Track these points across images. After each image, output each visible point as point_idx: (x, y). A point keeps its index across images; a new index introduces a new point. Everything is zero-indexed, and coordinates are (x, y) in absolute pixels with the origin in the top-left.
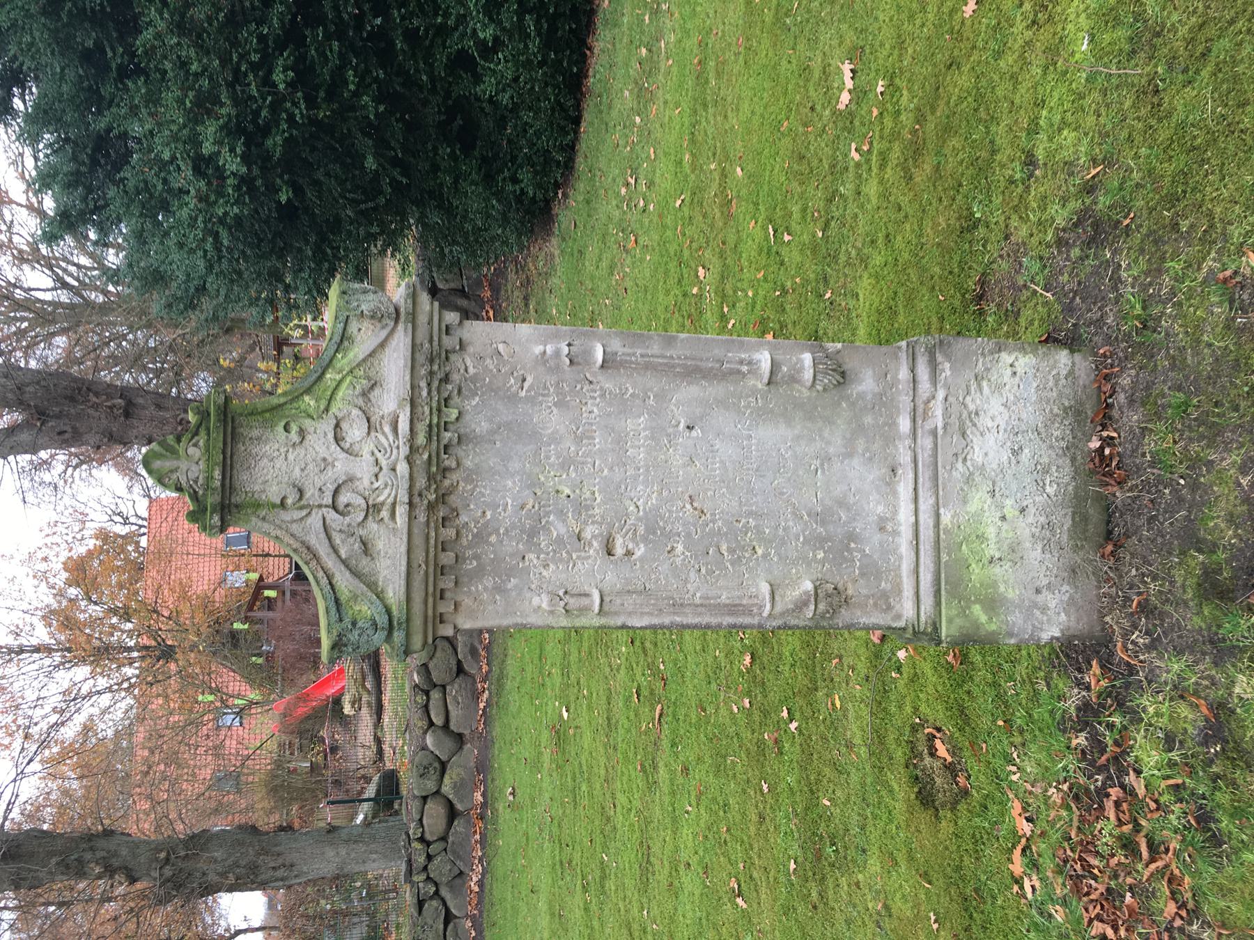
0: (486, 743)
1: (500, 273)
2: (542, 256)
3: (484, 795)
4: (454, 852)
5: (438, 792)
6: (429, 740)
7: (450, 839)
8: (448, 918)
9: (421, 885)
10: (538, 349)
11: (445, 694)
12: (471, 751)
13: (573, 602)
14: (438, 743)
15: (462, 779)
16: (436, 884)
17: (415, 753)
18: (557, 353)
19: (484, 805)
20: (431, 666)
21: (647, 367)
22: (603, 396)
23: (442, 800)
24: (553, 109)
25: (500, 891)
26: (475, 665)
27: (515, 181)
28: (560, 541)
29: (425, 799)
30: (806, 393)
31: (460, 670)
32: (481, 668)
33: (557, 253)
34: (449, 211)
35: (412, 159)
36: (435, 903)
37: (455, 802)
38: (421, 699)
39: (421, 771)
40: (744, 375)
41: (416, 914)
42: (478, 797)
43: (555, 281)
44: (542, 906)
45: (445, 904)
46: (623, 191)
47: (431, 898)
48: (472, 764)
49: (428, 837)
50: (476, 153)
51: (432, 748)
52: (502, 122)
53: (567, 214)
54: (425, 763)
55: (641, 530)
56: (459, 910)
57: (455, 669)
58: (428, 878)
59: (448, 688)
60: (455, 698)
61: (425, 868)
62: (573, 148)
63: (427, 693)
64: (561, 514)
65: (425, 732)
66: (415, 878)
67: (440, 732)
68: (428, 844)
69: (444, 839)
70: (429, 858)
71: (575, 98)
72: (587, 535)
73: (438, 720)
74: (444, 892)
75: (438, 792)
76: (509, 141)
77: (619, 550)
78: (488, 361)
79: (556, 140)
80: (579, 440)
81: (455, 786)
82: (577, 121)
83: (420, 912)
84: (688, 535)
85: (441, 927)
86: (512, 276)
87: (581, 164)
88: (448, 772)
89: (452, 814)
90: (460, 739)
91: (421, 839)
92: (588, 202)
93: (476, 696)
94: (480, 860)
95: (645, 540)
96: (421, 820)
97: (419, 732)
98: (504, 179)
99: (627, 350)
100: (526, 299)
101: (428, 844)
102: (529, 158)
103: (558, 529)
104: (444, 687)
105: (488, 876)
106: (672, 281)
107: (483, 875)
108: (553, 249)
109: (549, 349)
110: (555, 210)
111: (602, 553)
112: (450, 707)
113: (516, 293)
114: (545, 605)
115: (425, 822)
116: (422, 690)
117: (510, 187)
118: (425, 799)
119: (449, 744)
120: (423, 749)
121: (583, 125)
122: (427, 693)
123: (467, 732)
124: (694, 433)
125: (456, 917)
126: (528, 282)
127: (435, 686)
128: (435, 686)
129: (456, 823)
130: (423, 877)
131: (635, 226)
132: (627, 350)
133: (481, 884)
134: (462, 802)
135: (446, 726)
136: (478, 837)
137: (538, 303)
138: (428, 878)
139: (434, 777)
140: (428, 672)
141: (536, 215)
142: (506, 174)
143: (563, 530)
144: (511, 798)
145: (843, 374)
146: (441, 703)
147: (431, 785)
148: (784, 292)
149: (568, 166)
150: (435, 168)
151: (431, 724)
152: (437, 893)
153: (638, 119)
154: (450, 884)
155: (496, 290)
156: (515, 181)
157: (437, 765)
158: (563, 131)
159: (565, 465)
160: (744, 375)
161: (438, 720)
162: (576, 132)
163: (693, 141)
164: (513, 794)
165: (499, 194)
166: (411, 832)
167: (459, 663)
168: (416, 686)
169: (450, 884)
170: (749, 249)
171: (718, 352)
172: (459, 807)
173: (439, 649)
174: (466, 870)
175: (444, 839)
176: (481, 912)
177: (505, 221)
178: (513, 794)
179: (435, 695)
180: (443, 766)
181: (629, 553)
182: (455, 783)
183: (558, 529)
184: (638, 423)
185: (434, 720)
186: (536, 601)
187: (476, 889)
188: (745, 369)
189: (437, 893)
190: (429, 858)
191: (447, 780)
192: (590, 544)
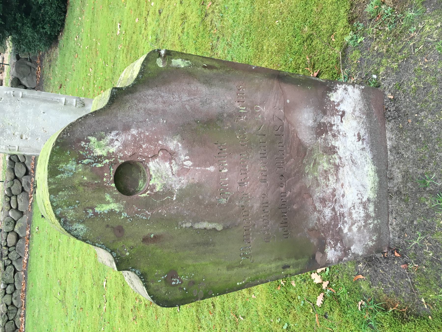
0: (31, 214)
1: (43, 55)
2: (55, 52)
3: (30, 232)
4: (18, 250)
5: (13, 231)
6: (10, 213)
7: (17, 246)
8: (15, 271)
9: (5, 261)
10: (5, 92)
11: (17, 198)
12: (26, 217)
13: (11, 148)
14: (13, 214)
15: (22, 226)
16: (11, 261)
17: (5, 218)
18: (10, 93)
19: (29, 235)
20: (12, 188)
21: (33, 98)
22: (22, 104)
23: (15, 233)
24: (57, 8)
25: (33, 260)
26: (28, 189)
27: (44, 28)
28: (9, 134)
29: (8, 233)
30: (75, 108)
31: (23, 190)
32: (31, 190)
33: (58, 53)
34: (20, 34)
35: (7, 15)
36: (10, 267)
37: (19, 234)
38: (8, 199)
39: (7, 223)
40: (58, 103)
41: (3, 270)
42: (28, 232)
43: (57, 63)
44: (44, 260)
45: (14, 267)
46: (76, 39)
47: (9, 265)
48: (26, 222)
49: (9, 245)
50: (30, 17)
51: (11, 216)
52: (40, 8)
53: (62, 40)
54: (9, 221)
55: (30, 134)
56: (20, 269)
57: (21, 189)
58: (8, 259)
59: (18, 196)
60: (20, 199)
61: (7, 255)
62: (64, 20)
63: (10, 198)
64: (9, 129)
65: (9, 211)
66: (3, 259)
67: (14, 211)
68: (9, 248)
69: (15, 246)
70: (9, 252)
71: (65, 5)
72: (16, 134)
73: (14, 206)
74: (14, 263)
75: (13, 231)
76: (42, 15)
77: (24, 138)
78: (389, 8)
79: (58, 17)
80: (15, 113)
81: (19, 229)
82: (65, 12)
83: (5, 269)
84: (42, 136)
85: (13, 274)
86: (46, 57)
87: (66, 27)
88: (17, 224)
89: (18, 238)
90: (22, 213)
91: (6, 246)
92: (67, 39)
93: (28, 199)
94: (28, 252)
95: (31, 136)
96: (6, 240)
97: (6, 210)
98: (40, 27)
99: (29, 94)
100: (50, 66)
101: (9, 248)
102: (49, 22)
103: (8, 132)
104: (17, 196)
105: (30, 257)
106: (84, 71)
107: (28, 257)
108: (57, 52)
109: (8, 92)
110: (59, 39)
111: (20, 138)
112: (18, 203)
113: (47, 64)
114: (4, 148)
115: (8, 240)
116: (8, 196)
117: (41, 30)
118: (8, 233)
119: (18, 215)
120: (8, 216)
121: (67, 14)
122: (10, 198)
123: (24, 211)
124: (45, 114)
125: (18, 271)
126: (50, 61)
127: (13, 195)
128: (13, 195)
129: (19, 241)
130: (6, 258)
131: (78, 51)
132: (29, 94)
133: (27, 260)
134: (22, 234)
135: (17, 209)
136: (27, 245)
137: (53, 68)
138: (8, 259)
139: (12, 226)
140: (11, 190)
141: (53, 39)
142: (40, 26)
143: (10, 132)
144: (37, 230)
145: (84, 105)
146: (15, 201)
147: (10, 228)
148: (106, 80)
149: (63, 26)
150: (15, 20)
151: (11, 208)
152: (11, 264)
153: (80, 18)
154: (16, 261)
155: (41, 61)
156: (44, 28)
157: (13, 221)
158: (60, 15)
159: (11, 118)
160: (58, 103)
161: (14, 206)
162: (65, 16)
163: (91, 31)
164: (38, 229)
165: (38, 32)
166: (2, 244)
167: (23, 188)
168: (6, 195)
169: (16, 261)
170: (100, 66)
171: (52, 97)
172: (21, 236)
173: (15, 183)
174: (22, 256)
175: (15, 246)
176: (27, 270)
177: (40, 41)
178: (38, 229)
179: (13, 198)
180: (15, 222)
181: (26, 139)
182: (19, 228)
183: (8, 132)
184: (30, 111)
185: (12, 207)
186: (2, 147)
187: (26, 262)
188: (58, 101)
189: (11, 264)
190: (9, 252)
191: (16, 227)
192: (17, 136)
